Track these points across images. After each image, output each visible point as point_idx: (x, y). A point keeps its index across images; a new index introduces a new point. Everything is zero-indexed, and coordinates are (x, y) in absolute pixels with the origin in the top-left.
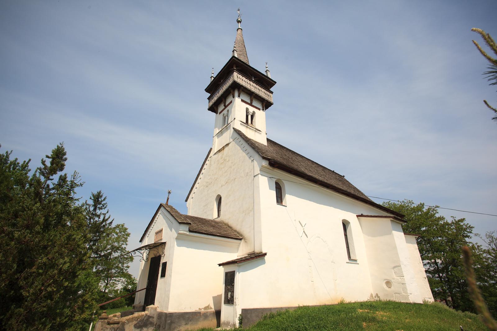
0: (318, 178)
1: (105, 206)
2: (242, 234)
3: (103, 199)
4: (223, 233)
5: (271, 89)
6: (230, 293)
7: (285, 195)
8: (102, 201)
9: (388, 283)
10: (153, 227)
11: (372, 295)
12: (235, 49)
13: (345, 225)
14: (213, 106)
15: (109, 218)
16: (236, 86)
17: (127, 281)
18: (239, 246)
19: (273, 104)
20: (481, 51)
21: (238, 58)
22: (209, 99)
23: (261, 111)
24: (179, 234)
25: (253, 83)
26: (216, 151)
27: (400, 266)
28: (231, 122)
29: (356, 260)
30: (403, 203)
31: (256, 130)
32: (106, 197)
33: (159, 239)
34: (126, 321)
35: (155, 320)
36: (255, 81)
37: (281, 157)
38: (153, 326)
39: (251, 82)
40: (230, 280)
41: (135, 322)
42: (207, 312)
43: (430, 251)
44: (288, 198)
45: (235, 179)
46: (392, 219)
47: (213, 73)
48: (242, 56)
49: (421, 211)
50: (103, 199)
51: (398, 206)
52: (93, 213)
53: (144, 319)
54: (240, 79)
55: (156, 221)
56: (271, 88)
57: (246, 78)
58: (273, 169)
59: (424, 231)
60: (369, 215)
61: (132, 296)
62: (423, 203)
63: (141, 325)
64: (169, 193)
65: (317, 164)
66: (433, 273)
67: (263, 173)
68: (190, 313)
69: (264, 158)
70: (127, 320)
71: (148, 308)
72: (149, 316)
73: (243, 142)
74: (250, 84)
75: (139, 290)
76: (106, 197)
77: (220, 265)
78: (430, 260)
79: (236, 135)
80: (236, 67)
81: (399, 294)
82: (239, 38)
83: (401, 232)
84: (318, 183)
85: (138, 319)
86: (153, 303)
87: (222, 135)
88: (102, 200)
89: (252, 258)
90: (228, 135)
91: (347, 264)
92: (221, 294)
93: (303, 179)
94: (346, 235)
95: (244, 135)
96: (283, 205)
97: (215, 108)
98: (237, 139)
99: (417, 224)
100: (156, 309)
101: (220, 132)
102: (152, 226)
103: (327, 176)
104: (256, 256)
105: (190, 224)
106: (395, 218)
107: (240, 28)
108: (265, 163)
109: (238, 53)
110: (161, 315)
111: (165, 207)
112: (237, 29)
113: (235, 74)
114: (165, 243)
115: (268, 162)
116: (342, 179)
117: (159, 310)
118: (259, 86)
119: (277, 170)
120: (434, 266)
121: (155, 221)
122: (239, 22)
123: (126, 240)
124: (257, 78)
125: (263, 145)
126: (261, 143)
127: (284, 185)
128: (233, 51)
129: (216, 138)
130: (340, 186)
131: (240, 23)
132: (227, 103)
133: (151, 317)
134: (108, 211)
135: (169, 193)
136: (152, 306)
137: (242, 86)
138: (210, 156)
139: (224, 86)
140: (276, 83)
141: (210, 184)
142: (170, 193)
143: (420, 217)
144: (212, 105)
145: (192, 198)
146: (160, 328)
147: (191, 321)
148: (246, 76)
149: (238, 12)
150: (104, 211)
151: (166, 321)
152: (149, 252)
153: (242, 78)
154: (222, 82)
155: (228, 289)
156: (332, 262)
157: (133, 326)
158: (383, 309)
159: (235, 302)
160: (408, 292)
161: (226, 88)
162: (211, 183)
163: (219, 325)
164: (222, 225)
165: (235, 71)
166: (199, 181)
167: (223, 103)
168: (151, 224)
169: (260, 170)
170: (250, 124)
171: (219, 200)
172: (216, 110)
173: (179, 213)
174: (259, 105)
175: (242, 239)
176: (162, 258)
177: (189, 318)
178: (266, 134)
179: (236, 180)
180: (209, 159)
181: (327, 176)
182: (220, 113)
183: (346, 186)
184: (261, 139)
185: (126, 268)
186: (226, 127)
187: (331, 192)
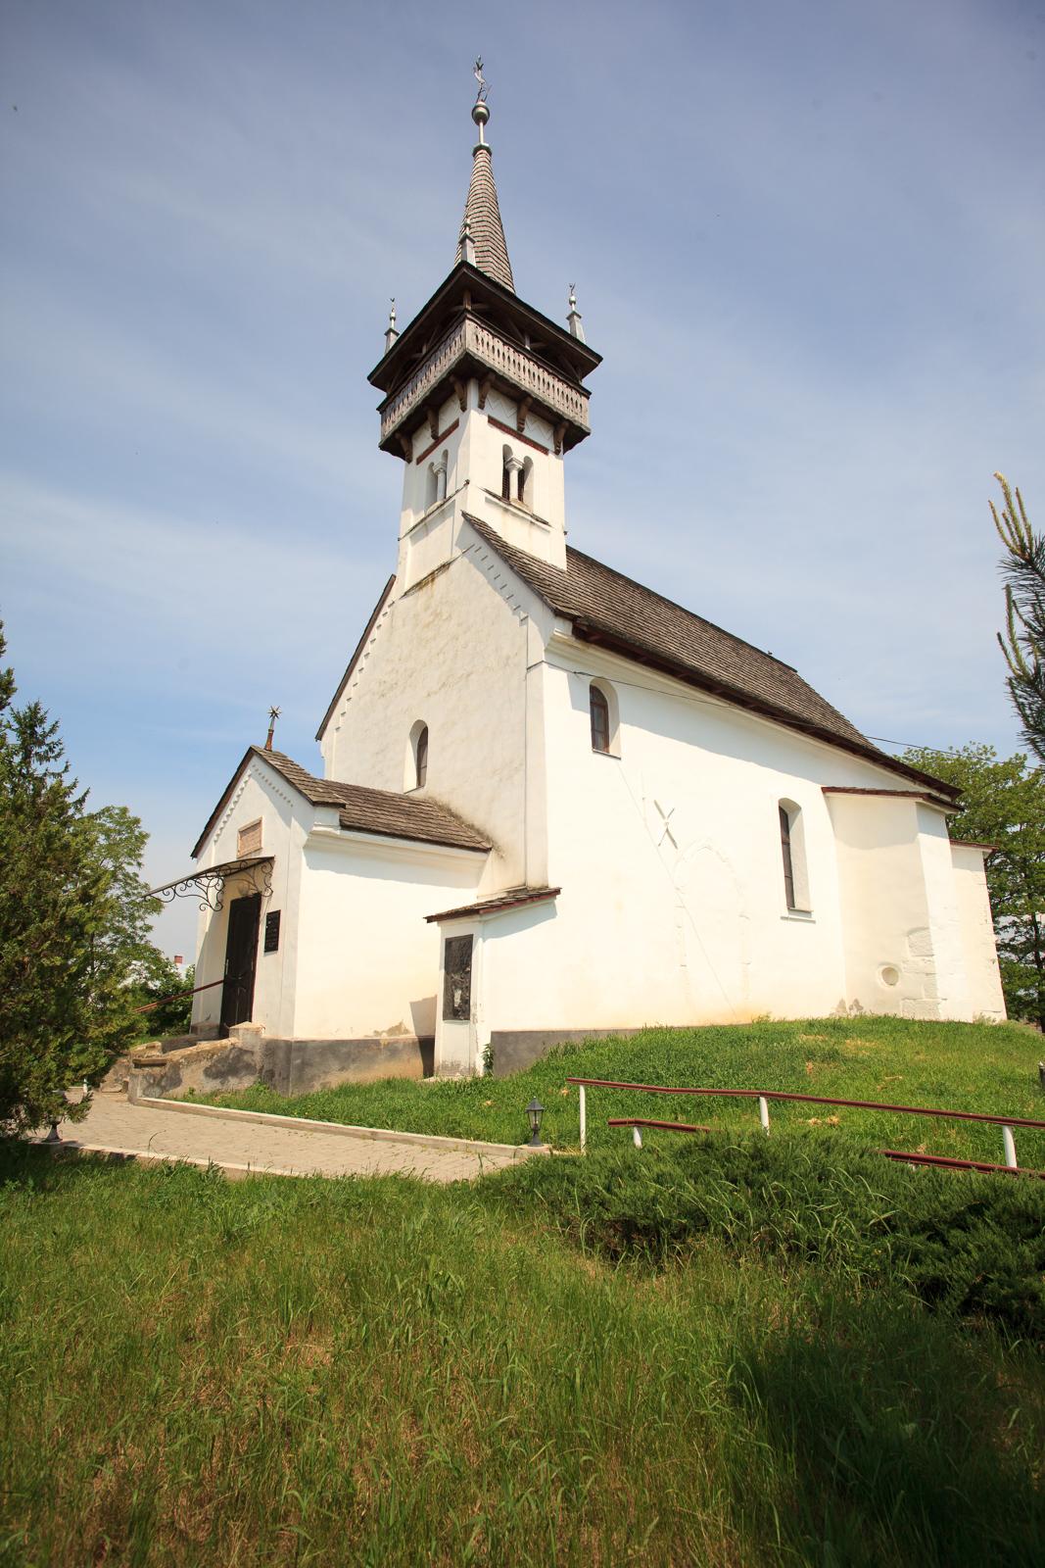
0: (716, 674)
1: (57, 751)
2: (490, 836)
3: (47, 726)
4: (438, 832)
5: (586, 383)
6: (460, 992)
7: (618, 725)
8: (45, 735)
9: (890, 973)
10: (228, 816)
11: (842, 1004)
12: (468, 232)
13: (787, 815)
14: (397, 435)
15: (74, 785)
16: (471, 371)
17: (147, 968)
18: (481, 869)
19: (589, 434)
20: (995, 516)
21: (481, 270)
22: (383, 409)
23: (551, 455)
24: (313, 834)
25: (526, 361)
26: (407, 587)
27: (928, 928)
28: (457, 492)
29: (808, 913)
30: (966, 754)
31: (534, 521)
32: (57, 723)
33: (251, 848)
34: (183, 1060)
35: (257, 1059)
36: (532, 355)
37: (608, 609)
38: (253, 1074)
39: (521, 356)
40: (458, 958)
41: (205, 1064)
42: (397, 1042)
43: (1025, 891)
44: (626, 735)
45: (468, 675)
46: (921, 800)
47: (394, 319)
48: (491, 259)
49: (1013, 778)
50: (47, 726)
51: (950, 762)
52: (20, 771)
53: (227, 1057)
54: (496, 352)
55: (239, 796)
56: (583, 377)
57: (505, 344)
58: (585, 648)
59: (1015, 835)
60: (859, 787)
61: (164, 1008)
62: (1025, 755)
63: (223, 1070)
64: (274, 714)
65: (718, 629)
66: (1021, 951)
67: (556, 661)
68: (351, 1041)
69: (558, 614)
70: (185, 1057)
71: (238, 1029)
72: (240, 1049)
73: (494, 559)
74: (517, 362)
75: (203, 985)
76: (57, 723)
77: (430, 919)
78: (1019, 915)
79: (473, 538)
80: (473, 301)
81: (914, 999)
82: (480, 185)
83: (942, 837)
84: (718, 691)
85: (213, 1055)
86: (246, 1015)
87: (427, 535)
88: (47, 730)
89: (520, 901)
90: (446, 536)
91: (782, 921)
92: (433, 996)
93: (670, 677)
94: (786, 843)
95: (498, 539)
96: (611, 754)
97: (403, 442)
98: (474, 548)
99: (997, 816)
100: (257, 1032)
101: (419, 523)
102: (228, 812)
103: (747, 668)
104: (531, 897)
105: (343, 806)
106: (929, 797)
107: (483, 144)
108: (562, 630)
109: (477, 244)
110: (272, 1048)
111: (267, 758)
112: (472, 152)
113: (470, 328)
114: (270, 860)
115: (571, 628)
116: (792, 676)
117: (266, 1035)
118: (547, 371)
119: (597, 650)
120: (1027, 932)
121: (234, 798)
122: (480, 118)
123: (134, 853)
124: (541, 341)
125: (555, 568)
126: (549, 562)
127: (615, 691)
128: (462, 242)
129: (407, 542)
130: (781, 699)
131: (484, 124)
132: (442, 429)
133: (246, 1052)
134: (67, 767)
135: (274, 714)
136: (245, 1025)
137: (491, 371)
138: (388, 601)
139: (433, 368)
140: (600, 359)
141: (392, 688)
142: (276, 715)
143: (1008, 796)
144: (394, 433)
145: (338, 729)
146: (273, 1076)
147: (354, 1061)
148: (504, 336)
149: (478, 76)
150: (55, 766)
151: (288, 1061)
152: (224, 885)
153: (491, 344)
154: (426, 354)
155: (454, 982)
156: (741, 916)
157: (201, 1071)
158: (863, 1033)
159: (475, 1015)
160: (939, 995)
161: (439, 375)
162: (396, 684)
163: (429, 1070)
164: (430, 809)
165: (469, 316)
166: (356, 676)
167: (428, 425)
168: (224, 807)
169: (546, 650)
170: (515, 501)
171: (422, 738)
172: (405, 449)
173: (306, 775)
174: (544, 437)
175: (491, 849)
176: (265, 901)
177: (348, 1055)
178: (565, 533)
179: (473, 677)
180: (385, 609)
181: (747, 668)
182: (420, 460)
183: (801, 700)
184: (548, 551)
185: (141, 933)
186: (440, 509)
187: (670, 683)
